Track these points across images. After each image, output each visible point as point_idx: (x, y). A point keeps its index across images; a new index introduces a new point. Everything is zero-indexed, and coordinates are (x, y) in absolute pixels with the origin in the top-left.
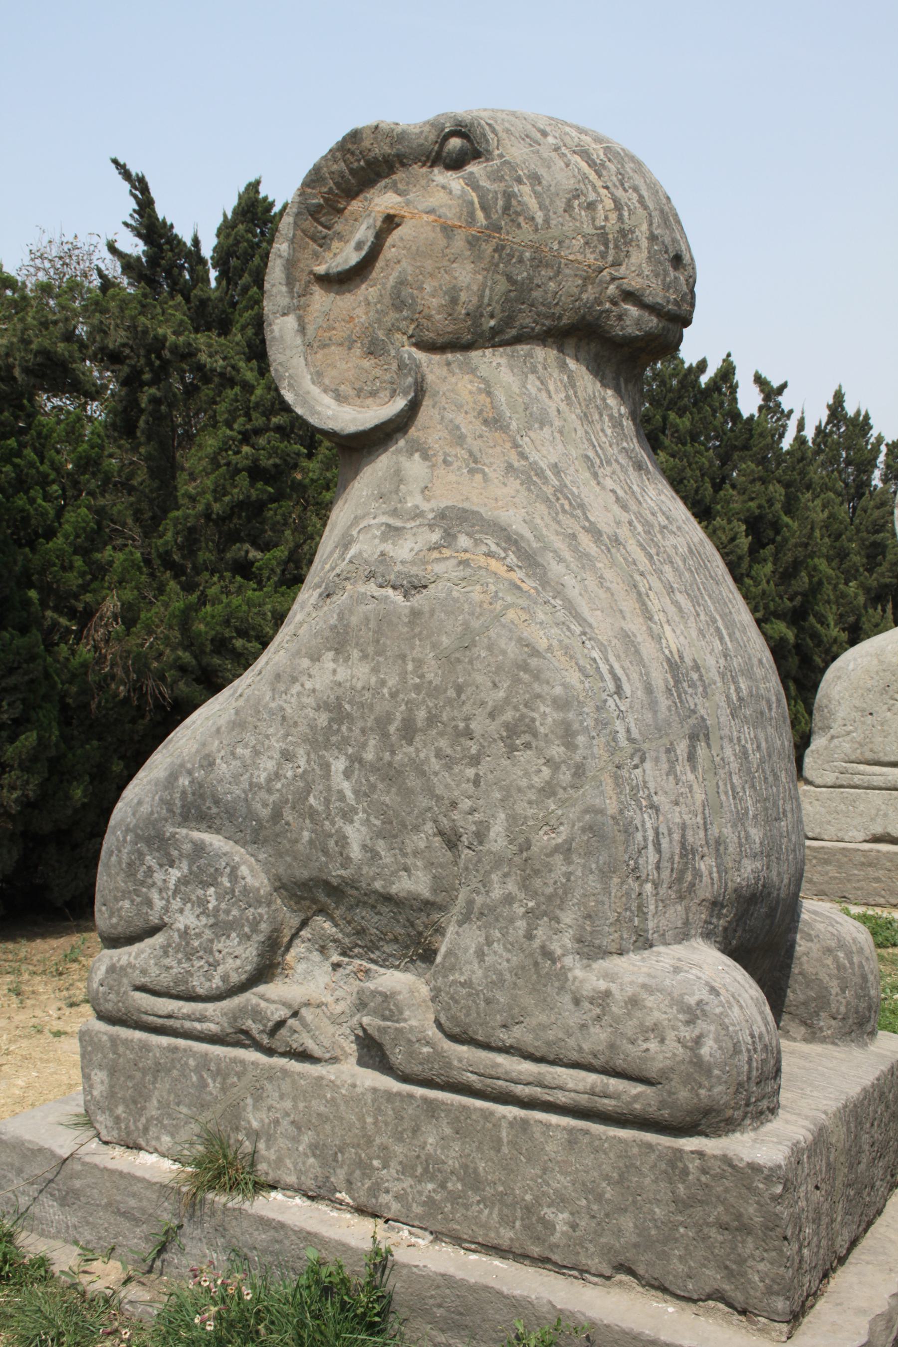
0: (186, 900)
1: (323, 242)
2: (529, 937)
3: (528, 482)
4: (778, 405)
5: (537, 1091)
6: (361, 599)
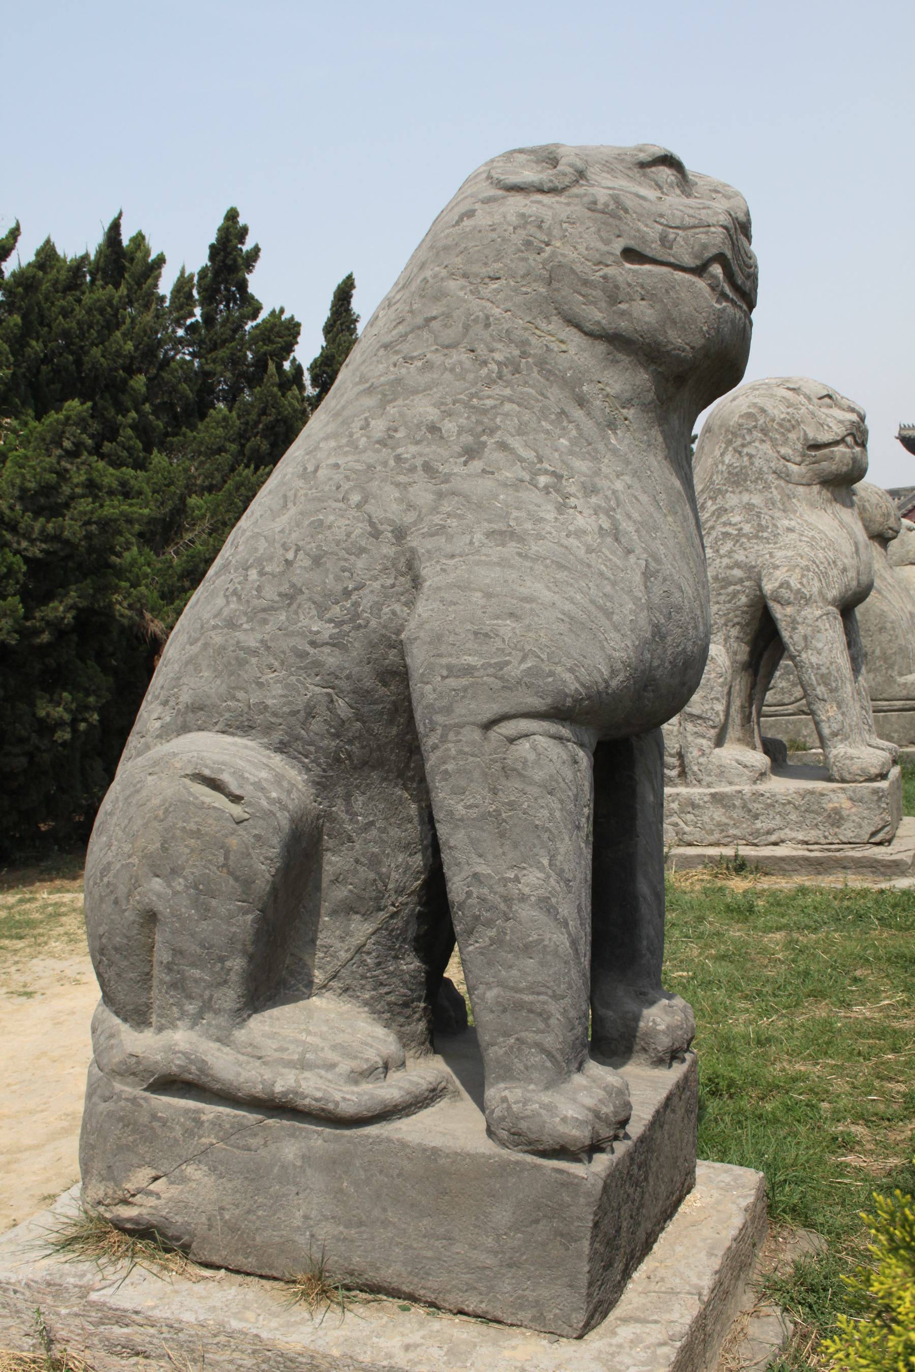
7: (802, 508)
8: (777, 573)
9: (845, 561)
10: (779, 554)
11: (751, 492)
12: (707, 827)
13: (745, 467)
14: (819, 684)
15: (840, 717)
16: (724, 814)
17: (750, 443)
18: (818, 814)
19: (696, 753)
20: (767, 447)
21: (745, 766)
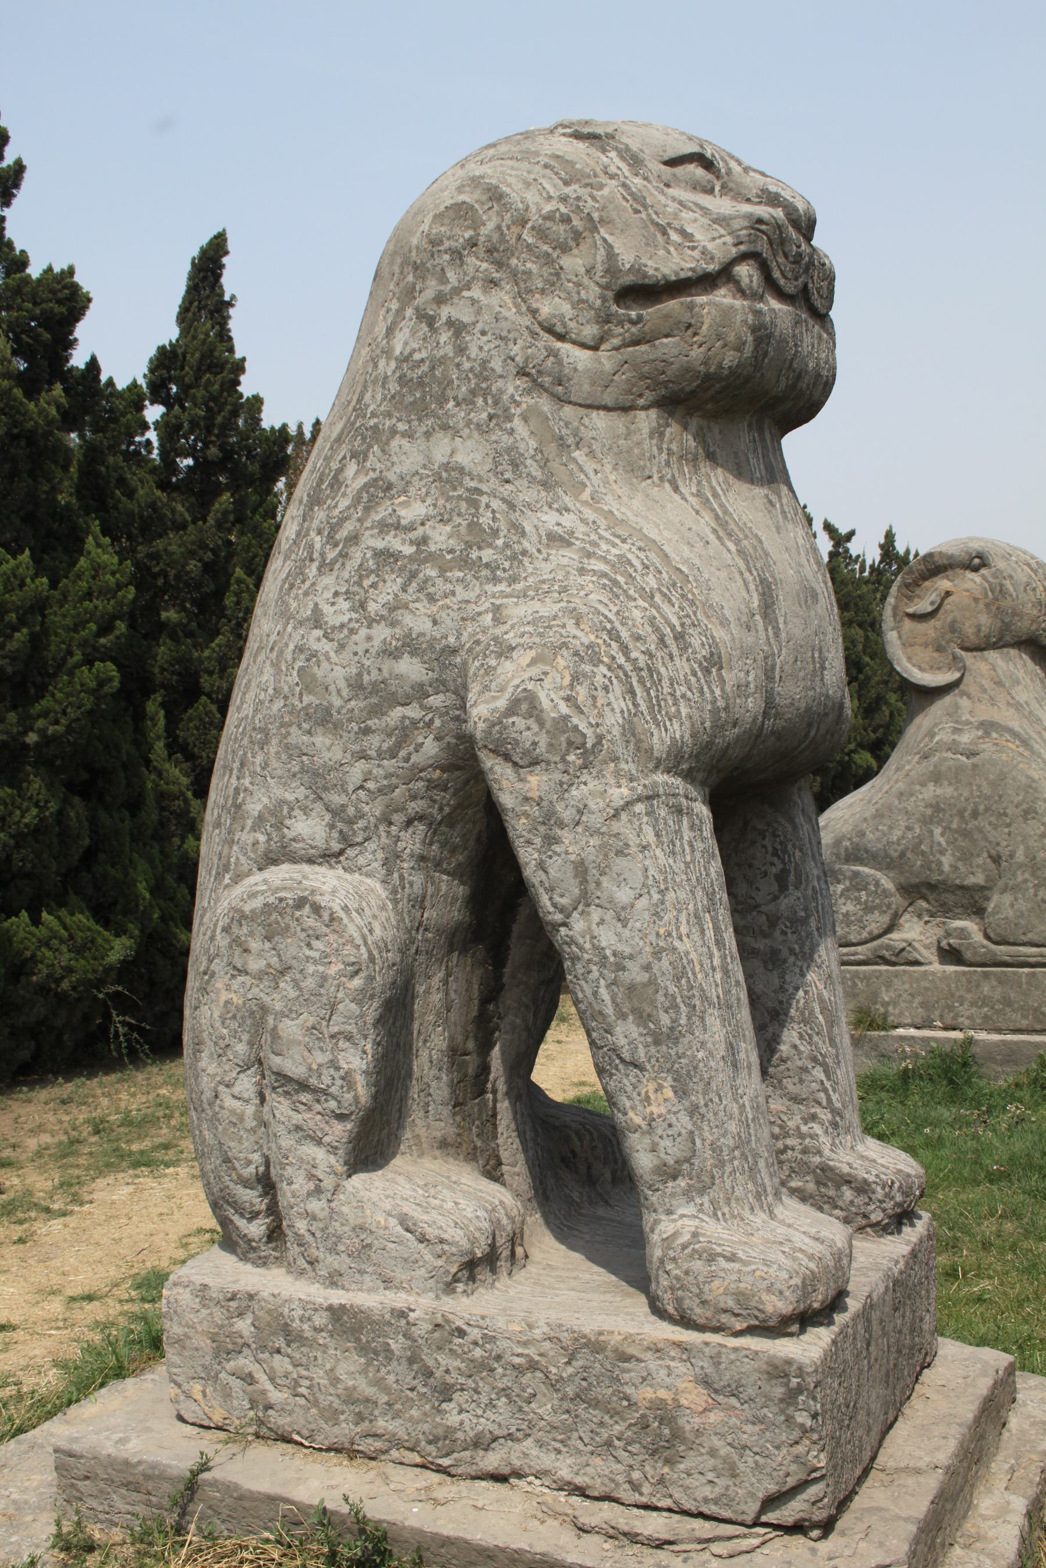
0: (847, 899)
1: (910, 599)
2: (1036, 895)
3: (1017, 709)
4: (847, 550)
5: (1040, 959)
6: (946, 759)
7: (601, 476)
8: (507, 667)
9: (719, 633)
10: (518, 611)
11: (456, 433)
12: (324, 1401)
13: (442, 361)
14: (623, 1016)
15: (684, 1122)
16: (364, 1372)
17: (457, 291)
18: (614, 1413)
19: (301, 1184)
20: (501, 300)
21: (423, 1239)
